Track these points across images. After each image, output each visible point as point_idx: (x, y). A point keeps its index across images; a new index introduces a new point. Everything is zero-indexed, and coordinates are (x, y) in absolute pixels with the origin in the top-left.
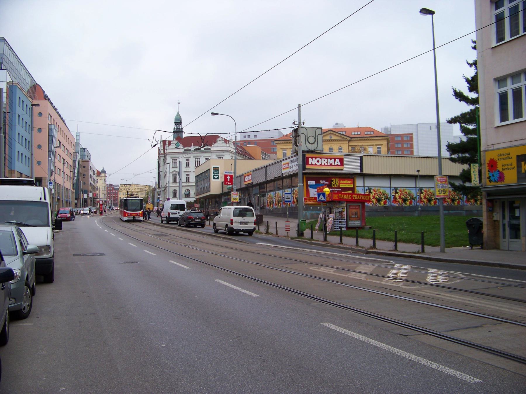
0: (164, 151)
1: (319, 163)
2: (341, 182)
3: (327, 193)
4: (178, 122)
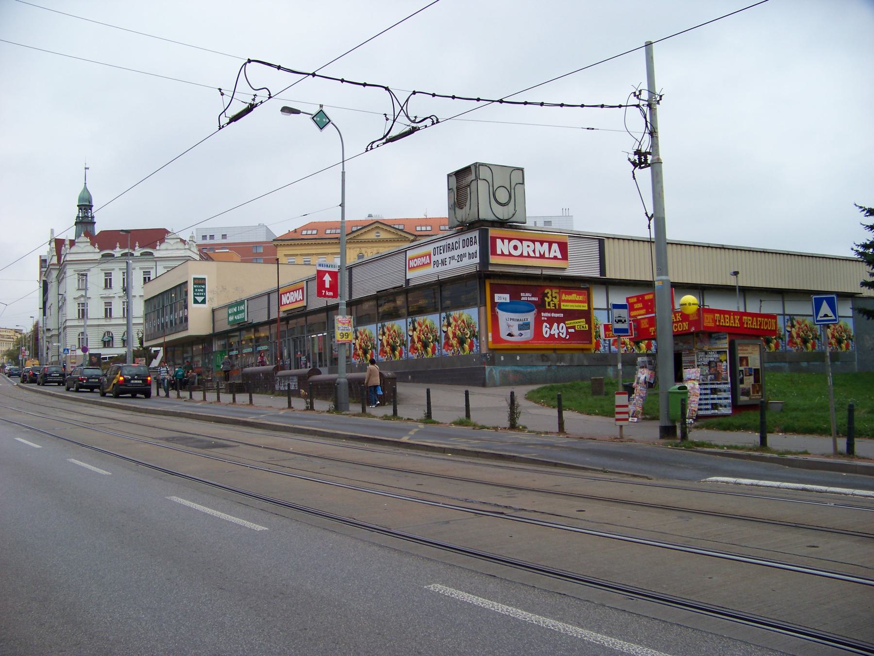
0: (59, 259)
1: (518, 253)
2: (564, 297)
3: (692, 310)
4: (85, 206)
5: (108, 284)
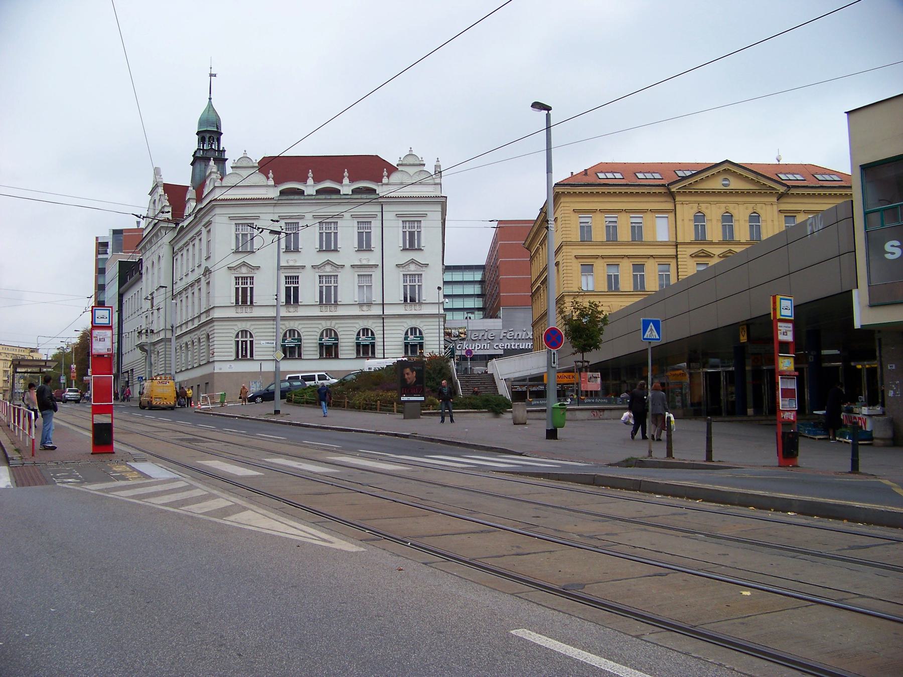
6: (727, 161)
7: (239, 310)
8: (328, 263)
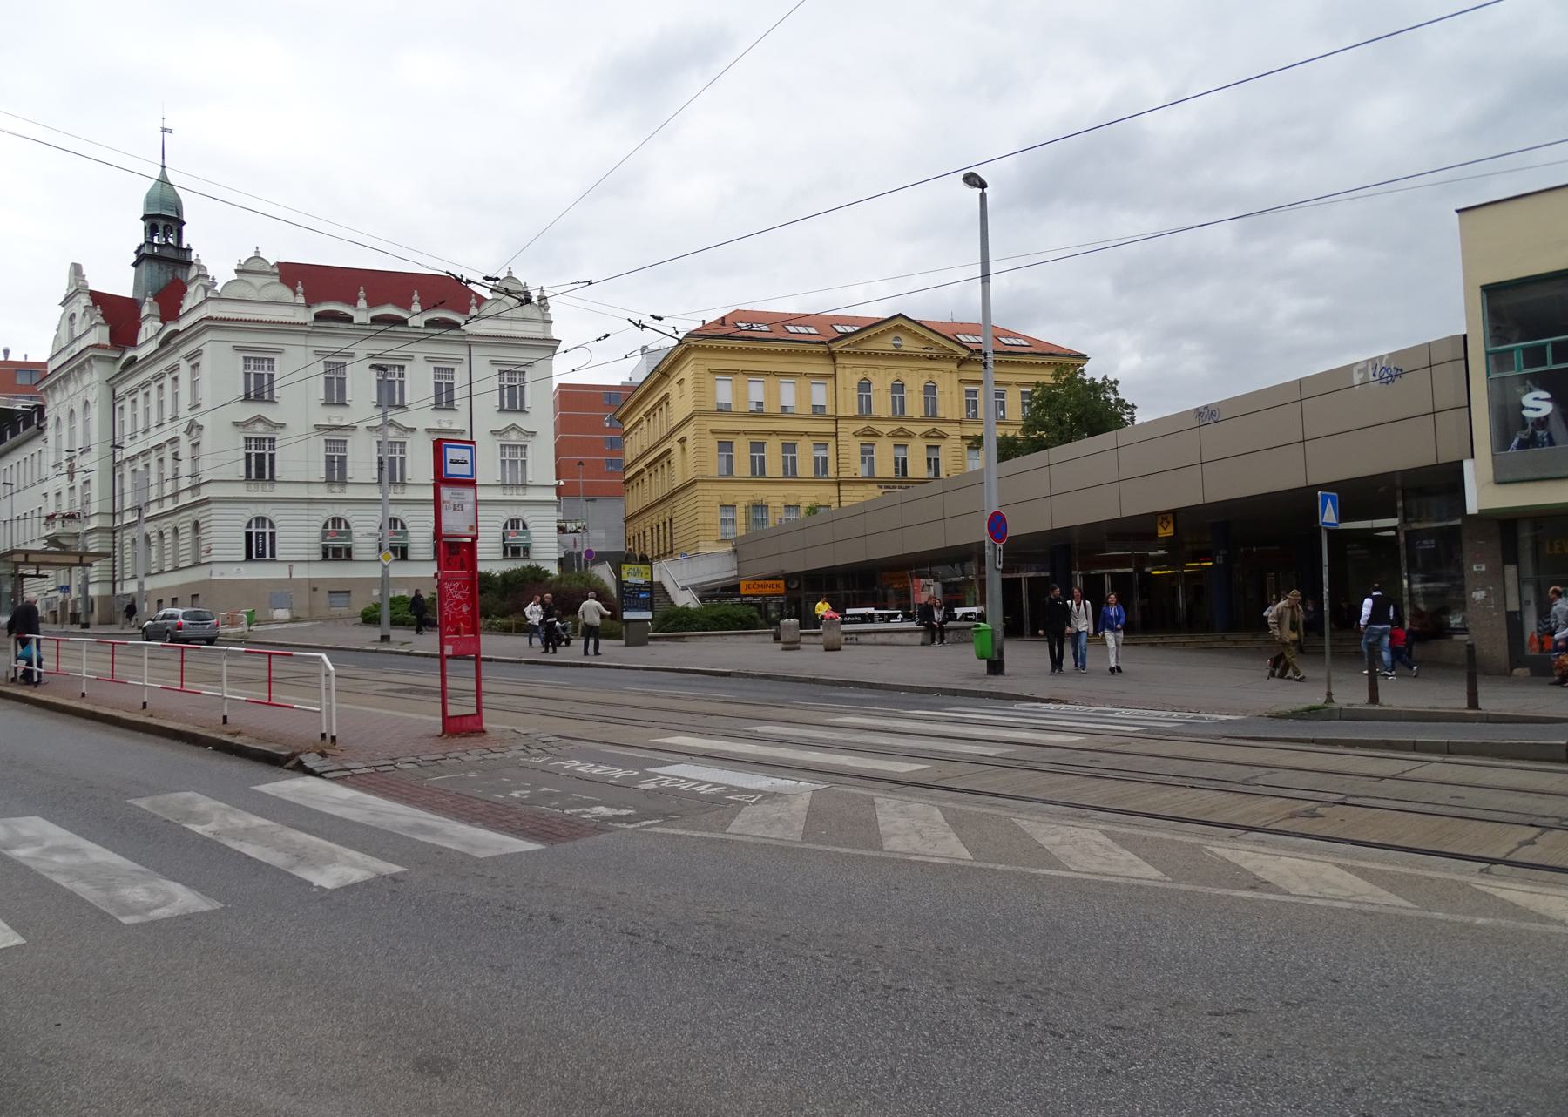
4: (164, 219)
5: (335, 395)
6: (900, 315)
7: (252, 487)
8: (514, 428)
